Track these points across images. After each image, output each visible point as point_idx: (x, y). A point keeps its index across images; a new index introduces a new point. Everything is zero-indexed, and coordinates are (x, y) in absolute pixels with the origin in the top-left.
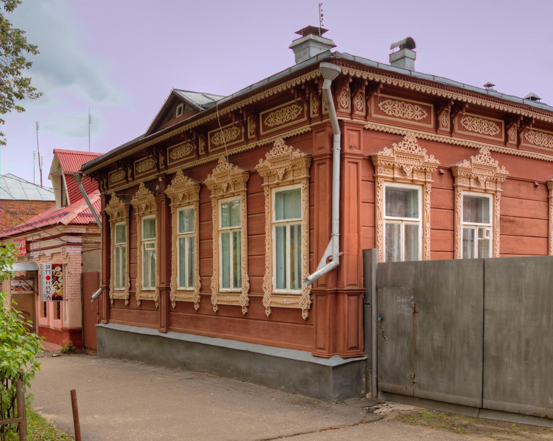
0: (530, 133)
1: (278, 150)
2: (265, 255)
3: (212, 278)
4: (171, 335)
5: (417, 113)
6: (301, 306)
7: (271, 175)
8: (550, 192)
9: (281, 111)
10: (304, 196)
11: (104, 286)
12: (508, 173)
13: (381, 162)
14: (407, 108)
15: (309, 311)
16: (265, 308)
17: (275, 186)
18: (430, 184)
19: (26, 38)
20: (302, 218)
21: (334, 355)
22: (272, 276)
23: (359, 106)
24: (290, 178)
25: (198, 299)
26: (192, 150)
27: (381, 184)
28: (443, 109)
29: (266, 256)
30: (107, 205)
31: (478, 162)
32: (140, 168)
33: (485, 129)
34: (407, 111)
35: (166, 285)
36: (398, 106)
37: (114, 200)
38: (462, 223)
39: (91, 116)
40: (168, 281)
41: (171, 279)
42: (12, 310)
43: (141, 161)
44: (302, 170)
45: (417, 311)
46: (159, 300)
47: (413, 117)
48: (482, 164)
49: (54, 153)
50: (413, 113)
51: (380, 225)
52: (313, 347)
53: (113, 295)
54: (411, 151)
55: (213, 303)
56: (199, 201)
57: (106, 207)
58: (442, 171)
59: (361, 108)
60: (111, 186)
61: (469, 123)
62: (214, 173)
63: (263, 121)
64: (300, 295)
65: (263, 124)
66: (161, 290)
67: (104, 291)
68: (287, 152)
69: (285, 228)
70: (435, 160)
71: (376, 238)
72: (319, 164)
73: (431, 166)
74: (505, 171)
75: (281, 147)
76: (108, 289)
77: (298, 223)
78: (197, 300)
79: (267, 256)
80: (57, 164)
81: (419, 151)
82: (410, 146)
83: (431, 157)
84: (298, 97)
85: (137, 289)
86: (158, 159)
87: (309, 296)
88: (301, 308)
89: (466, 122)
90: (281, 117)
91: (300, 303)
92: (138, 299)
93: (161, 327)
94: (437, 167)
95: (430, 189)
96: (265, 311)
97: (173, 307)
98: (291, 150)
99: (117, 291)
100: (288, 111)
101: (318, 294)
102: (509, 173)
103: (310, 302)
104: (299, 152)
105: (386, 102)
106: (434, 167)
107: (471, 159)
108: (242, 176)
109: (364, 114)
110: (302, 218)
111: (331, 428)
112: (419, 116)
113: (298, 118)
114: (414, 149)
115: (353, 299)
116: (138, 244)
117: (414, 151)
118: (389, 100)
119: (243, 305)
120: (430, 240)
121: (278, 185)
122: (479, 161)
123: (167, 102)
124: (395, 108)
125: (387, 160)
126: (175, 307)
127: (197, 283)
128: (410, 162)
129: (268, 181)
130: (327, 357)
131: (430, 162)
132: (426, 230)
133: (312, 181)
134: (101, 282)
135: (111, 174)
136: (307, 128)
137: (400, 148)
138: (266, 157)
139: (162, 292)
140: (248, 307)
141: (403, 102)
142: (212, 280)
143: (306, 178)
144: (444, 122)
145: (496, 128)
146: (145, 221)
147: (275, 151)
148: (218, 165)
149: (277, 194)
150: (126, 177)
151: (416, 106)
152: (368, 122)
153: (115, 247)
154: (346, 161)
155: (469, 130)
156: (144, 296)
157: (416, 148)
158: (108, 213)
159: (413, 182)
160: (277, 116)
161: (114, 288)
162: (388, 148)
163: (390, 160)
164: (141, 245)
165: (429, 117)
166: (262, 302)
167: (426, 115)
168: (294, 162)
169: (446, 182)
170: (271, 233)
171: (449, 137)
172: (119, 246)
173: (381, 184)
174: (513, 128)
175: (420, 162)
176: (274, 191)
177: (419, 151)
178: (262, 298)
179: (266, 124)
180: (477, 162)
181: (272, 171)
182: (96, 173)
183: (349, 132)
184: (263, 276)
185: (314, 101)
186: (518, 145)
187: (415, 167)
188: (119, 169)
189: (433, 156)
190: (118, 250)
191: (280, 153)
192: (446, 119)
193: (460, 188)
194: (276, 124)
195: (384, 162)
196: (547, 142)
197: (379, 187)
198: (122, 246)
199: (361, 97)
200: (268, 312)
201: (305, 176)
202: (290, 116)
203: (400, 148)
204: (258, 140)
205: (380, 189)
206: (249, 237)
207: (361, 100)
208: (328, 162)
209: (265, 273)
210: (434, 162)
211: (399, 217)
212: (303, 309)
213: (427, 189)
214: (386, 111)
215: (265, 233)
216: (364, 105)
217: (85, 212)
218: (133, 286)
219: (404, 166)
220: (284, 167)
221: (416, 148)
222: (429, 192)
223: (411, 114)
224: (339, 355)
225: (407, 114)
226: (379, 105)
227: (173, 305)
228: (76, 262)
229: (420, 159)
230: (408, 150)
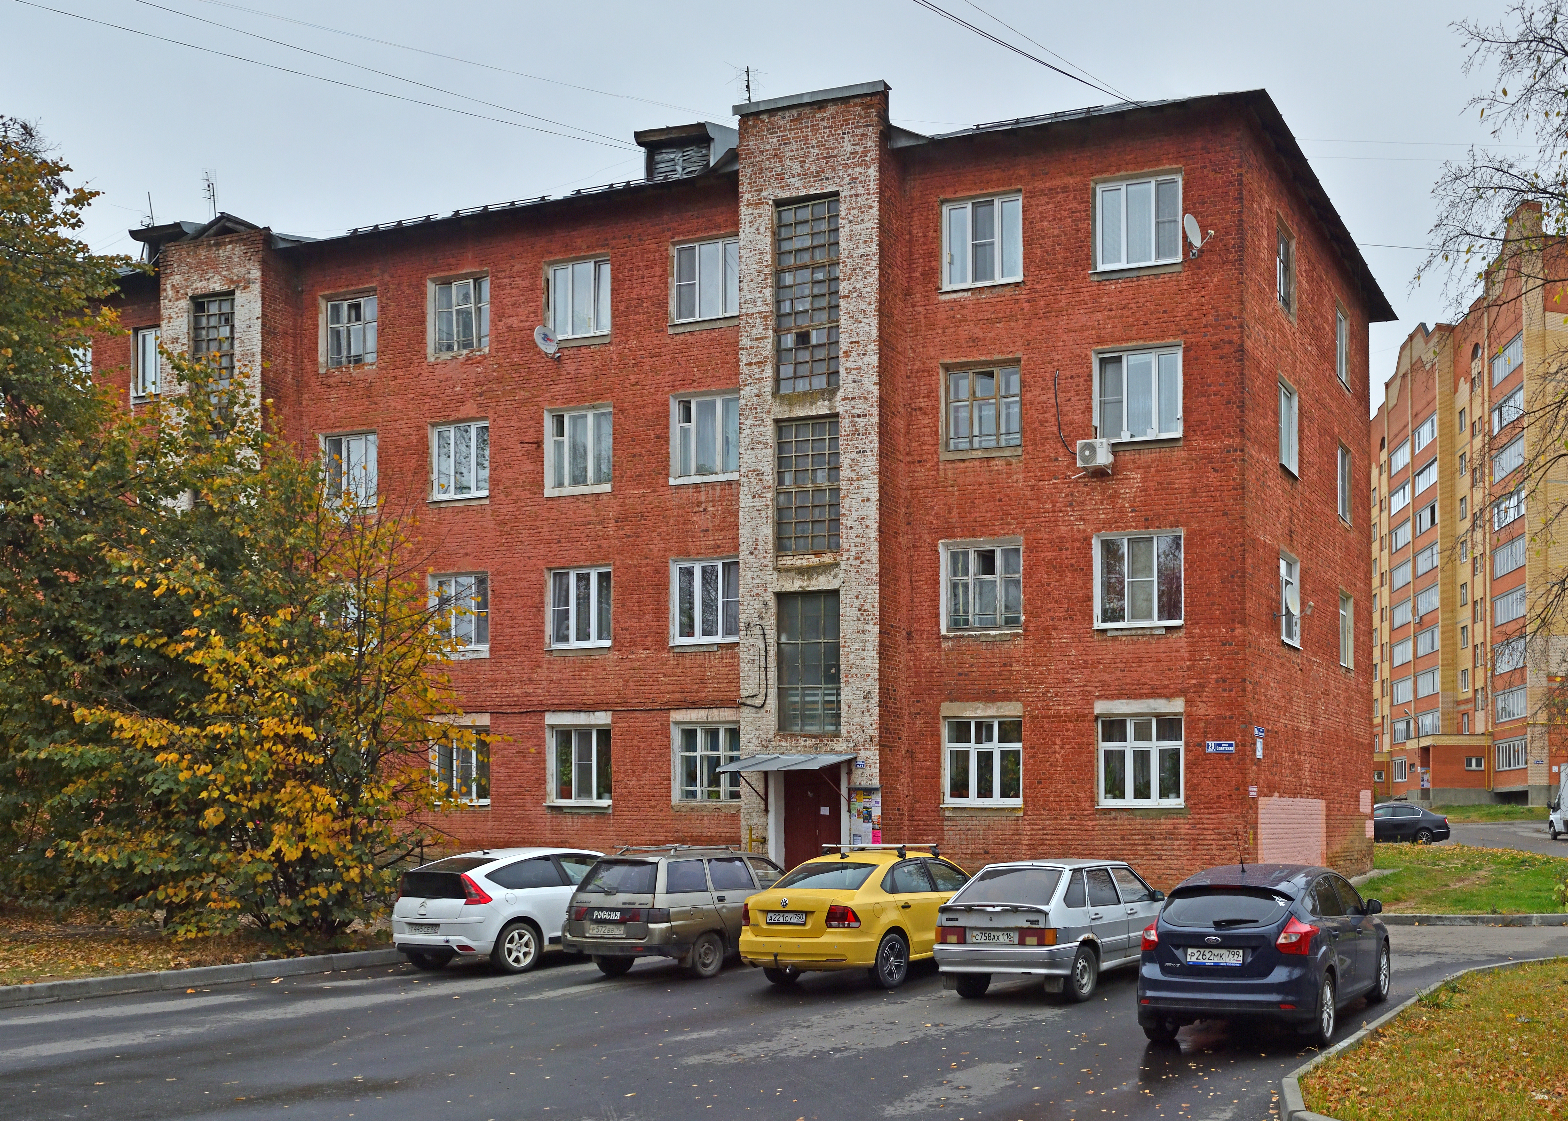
19: (89, 205)
28: (316, 300)
38: (1068, 867)
39: (207, 194)
42: (931, 326)
101: (952, 397)
111: (1473, 806)
115: (787, 284)
119: (1263, 801)
123: (1381, 294)
182: (84, 878)
211: (1161, 780)
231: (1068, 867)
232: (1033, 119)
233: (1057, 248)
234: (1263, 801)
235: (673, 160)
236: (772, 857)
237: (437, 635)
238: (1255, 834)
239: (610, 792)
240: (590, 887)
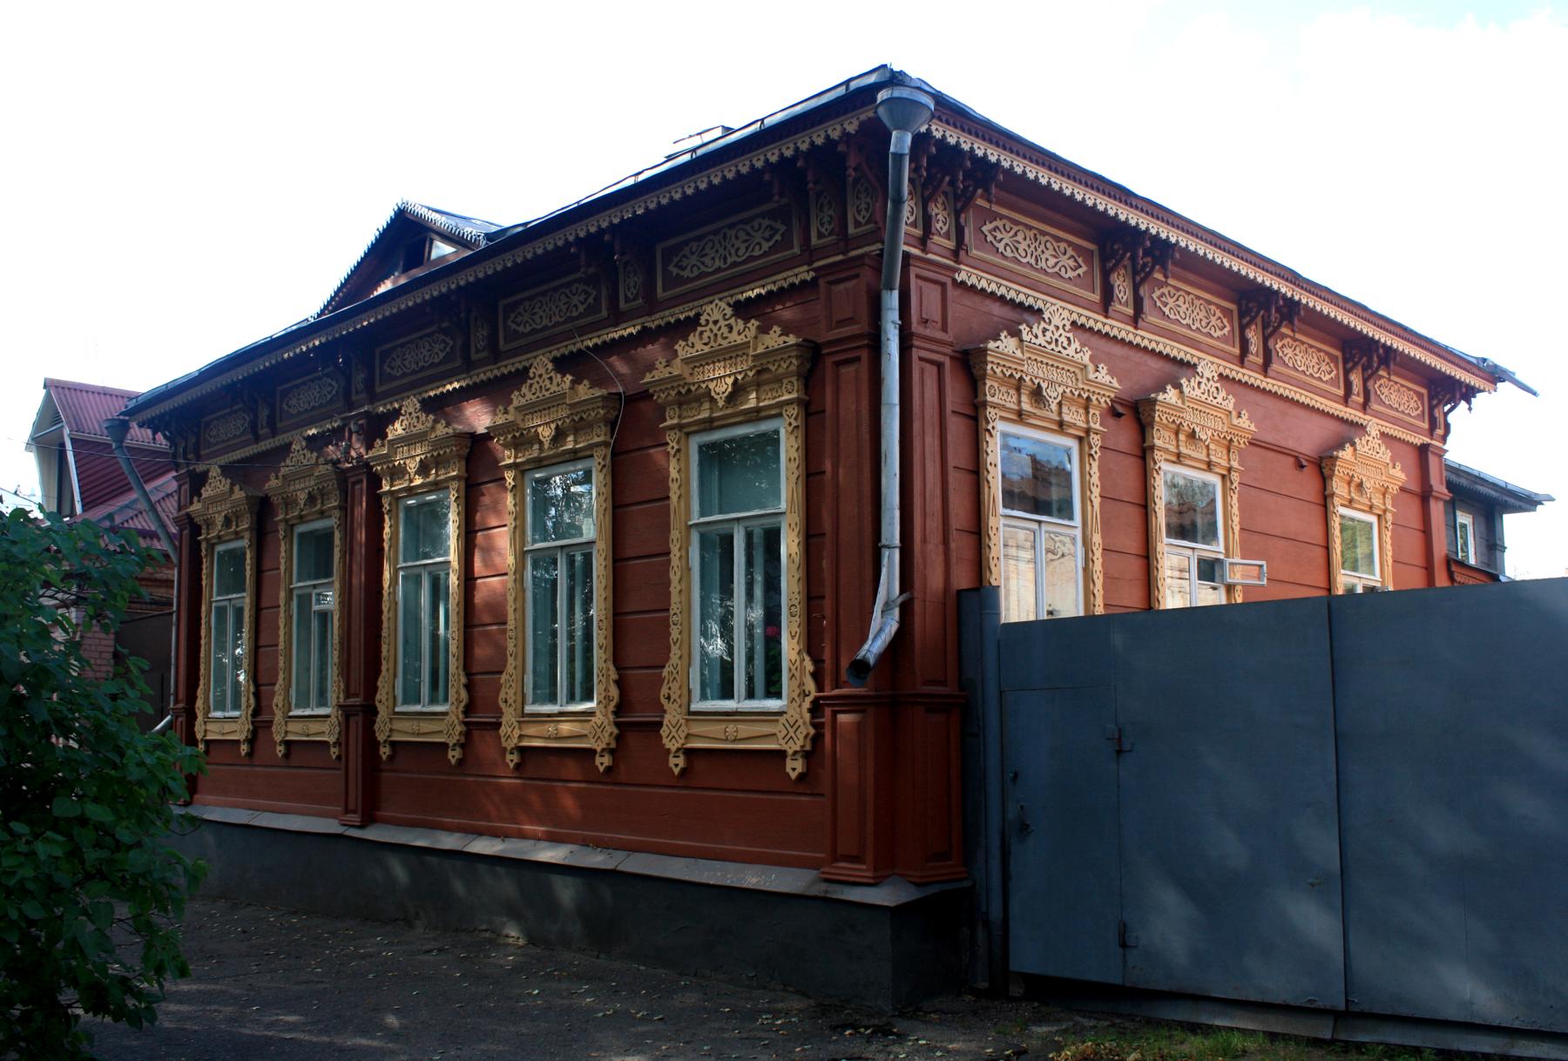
0: (1285, 341)
1: (715, 331)
2: (668, 610)
3: (504, 677)
4: (374, 834)
5: (1065, 260)
6: (783, 742)
7: (691, 397)
8: (1328, 482)
9: (722, 235)
10: (789, 449)
11: (181, 705)
12: (1253, 428)
13: (995, 367)
14: (1042, 247)
15: (807, 756)
16: (668, 751)
17: (702, 427)
18: (1098, 437)
20: (783, 506)
21: (889, 876)
22: (689, 665)
23: (941, 224)
24: (752, 401)
25: (461, 733)
26: (448, 349)
27: (994, 424)
29: (672, 612)
30: (195, 499)
31: (1195, 393)
32: (294, 402)
33: (1201, 320)
34: (1043, 252)
35: (365, 699)
36: (1025, 239)
37: (216, 485)
40: (372, 689)
41: (379, 684)
43: (297, 386)
44: (785, 381)
45: (1127, 747)
46: (343, 740)
47: (1056, 269)
48: (1203, 399)
49: (45, 387)
50: (1056, 260)
51: (994, 529)
52: (823, 855)
53: (206, 731)
54: (1060, 348)
55: (504, 744)
56: (467, 480)
57: (191, 503)
58: (1120, 409)
59: (945, 229)
60: (207, 451)
61: (1171, 301)
62: (516, 403)
63: (666, 263)
64: (780, 714)
65: (665, 271)
66: (347, 712)
67: (180, 719)
68: (742, 336)
69: (728, 541)
70: (1108, 378)
71: (984, 563)
72: (838, 364)
73: (1102, 392)
74: (1248, 422)
75: (722, 323)
76: (191, 717)
77: (768, 522)
78: (457, 738)
79: (676, 611)
80: (50, 416)
81: (1077, 353)
82: (1056, 336)
83: (1100, 369)
84: (781, 195)
85: (276, 711)
86: (349, 379)
87: (807, 716)
88: (785, 747)
89: (1163, 299)
90: (721, 251)
91: (780, 736)
92: (278, 738)
93: (347, 811)
94: (1112, 395)
95: (1097, 449)
96: (667, 761)
97: (384, 757)
98: (753, 329)
99: (217, 720)
100: (742, 236)
102: (1256, 426)
103: (812, 731)
104: (779, 332)
105: (998, 223)
106: (1107, 394)
107: (1181, 385)
108: (600, 404)
109: (951, 244)
110: (783, 506)
112: (1069, 269)
113: (773, 250)
114: (1065, 344)
116: (282, 594)
117: (1065, 348)
118: (1004, 221)
120: (1101, 577)
121: (709, 425)
122: (1198, 392)
124: (1019, 243)
125: (1008, 364)
126: (391, 758)
127: (458, 692)
128: (1054, 375)
129: (679, 417)
130: (871, 881)
131: (1098, 380)
132: (1092, 551)
133: (813, 409)
134: (172, 698)
135: (208, 425)
136: (803, 274)
137: (1036, 337)
138: (676, 351)
139: (353, 720)
140: (612, 752)
141: (1034, 231)
142: (502, 681)
143: (798, 401)
144: (1120, 291)
145: (1222, 322)
146: (301, 535)
147: (705, 335)
148: (529, 382)
149: (705, 450)
150: (254, 427)
151: (1063, 245)
152: (962, 267)
153: (214, 604)
154: (915, 353)
155: (1172, 316)
156: (296, 732)
157: (1069, 344)
158: (197, 520)
159: (1061, 426)
160: (707, 250)
161: (209, 712)
162: (1009, 334)
163: (1014, 366)
164: (291, 599)
165: (1091, 272)
166: (661, 737)
167: (1084, 268)
168: (764, 361)
169: (1124, 436)
170: (687, 553)
171: (1131, 329)
172: (227, 603)
173: (994, 424)
174: (1253, 327)
175: (1077, 380)
176: (694, 443)
177: (1077, 353)
178: (660, 724)
179: (675, 271)
180: (1193, 394)
181: (693, 388)
183: (921, 283)
184: (663, 667)
185: (822, 206)
186: (1265, 368)
187: (1068, 391)
188: (236, 407)
189: (1105, 368)
190: (221, 612)
191: (720, 340)
192: (1125, 284)
193: (1159, 453)
194: (703, 269)
195: (1000, 369)
196: (1317, 367)
197: (988, 430)
198: (232, 602)
199: (943, 203)
200: (677, 763)
201: (794, 395)
202: (747, 248)
203: (1036, 337)
204: (650, 314)
205: (991, 435)
206: (618, 564)
207: (945, 209)
208: (864, 355)
209: (668, 658)
210: (1108, 383)
212: (790, 752)
213: (1091, 448)
214: (1001, 246)
215: (669, 553)
216: (951, 221)
217: (126, 525)
218: (264, 703)
219: (1044, 385)
220: (729, 376)
221: (1069, 344)
222: (1096, 457)
223: (1052, 261)
224: (902, 875)
225: (1043, 260)
226: (985, 229)
227: (385, 752)
228: (100, 649)
229: (1077, 371)
230: (1053, 346)
231: (579, 553)
232: (1121, 194)
233: (435, 1022)
234: (332, 739)
235: (221, 612)
236: (1472, 561)
237: (103, 854)
238: (1481, 377)
239: (1259, 1051)
240: (919, 281)
